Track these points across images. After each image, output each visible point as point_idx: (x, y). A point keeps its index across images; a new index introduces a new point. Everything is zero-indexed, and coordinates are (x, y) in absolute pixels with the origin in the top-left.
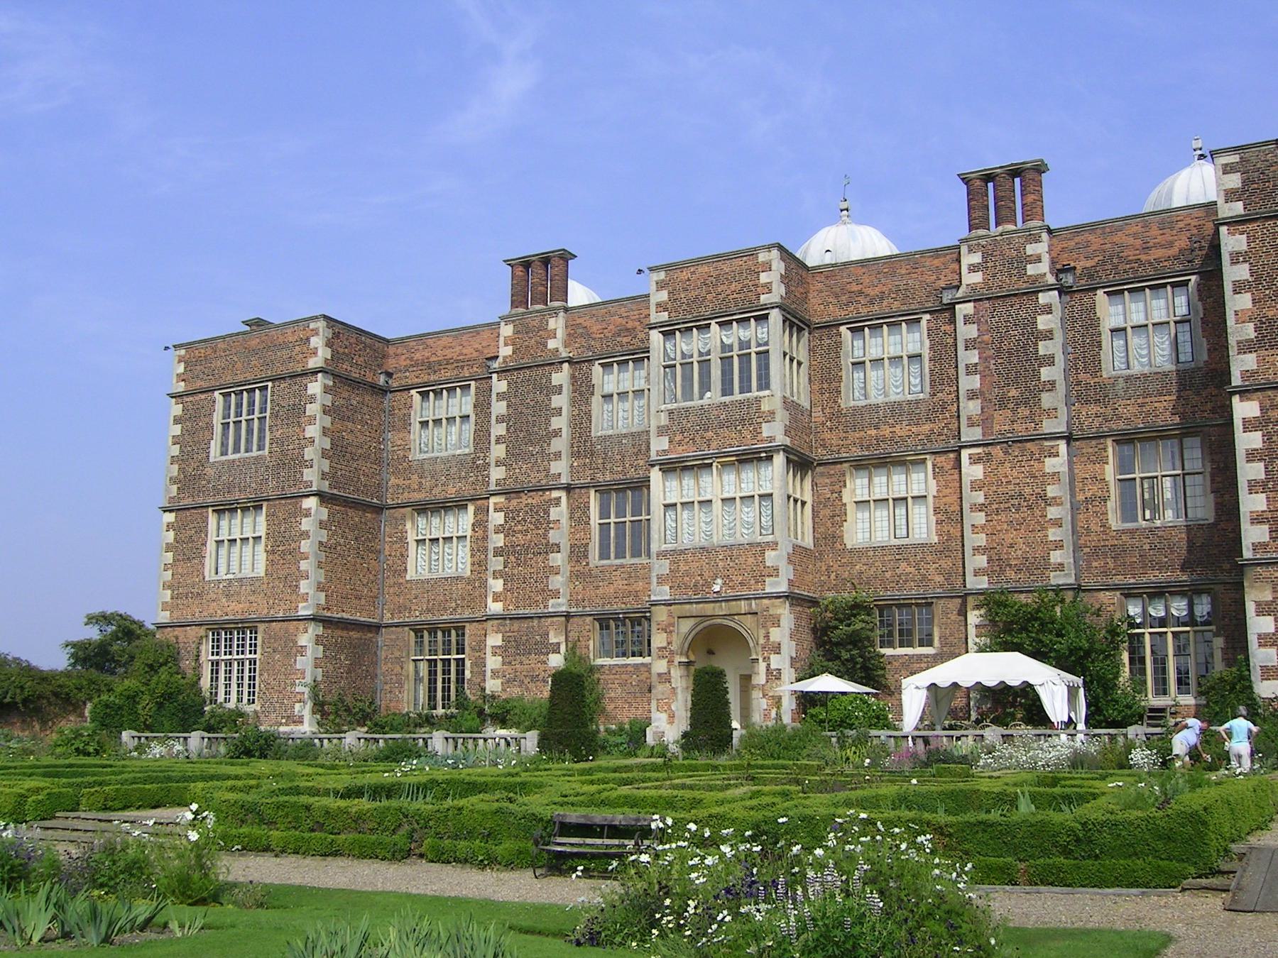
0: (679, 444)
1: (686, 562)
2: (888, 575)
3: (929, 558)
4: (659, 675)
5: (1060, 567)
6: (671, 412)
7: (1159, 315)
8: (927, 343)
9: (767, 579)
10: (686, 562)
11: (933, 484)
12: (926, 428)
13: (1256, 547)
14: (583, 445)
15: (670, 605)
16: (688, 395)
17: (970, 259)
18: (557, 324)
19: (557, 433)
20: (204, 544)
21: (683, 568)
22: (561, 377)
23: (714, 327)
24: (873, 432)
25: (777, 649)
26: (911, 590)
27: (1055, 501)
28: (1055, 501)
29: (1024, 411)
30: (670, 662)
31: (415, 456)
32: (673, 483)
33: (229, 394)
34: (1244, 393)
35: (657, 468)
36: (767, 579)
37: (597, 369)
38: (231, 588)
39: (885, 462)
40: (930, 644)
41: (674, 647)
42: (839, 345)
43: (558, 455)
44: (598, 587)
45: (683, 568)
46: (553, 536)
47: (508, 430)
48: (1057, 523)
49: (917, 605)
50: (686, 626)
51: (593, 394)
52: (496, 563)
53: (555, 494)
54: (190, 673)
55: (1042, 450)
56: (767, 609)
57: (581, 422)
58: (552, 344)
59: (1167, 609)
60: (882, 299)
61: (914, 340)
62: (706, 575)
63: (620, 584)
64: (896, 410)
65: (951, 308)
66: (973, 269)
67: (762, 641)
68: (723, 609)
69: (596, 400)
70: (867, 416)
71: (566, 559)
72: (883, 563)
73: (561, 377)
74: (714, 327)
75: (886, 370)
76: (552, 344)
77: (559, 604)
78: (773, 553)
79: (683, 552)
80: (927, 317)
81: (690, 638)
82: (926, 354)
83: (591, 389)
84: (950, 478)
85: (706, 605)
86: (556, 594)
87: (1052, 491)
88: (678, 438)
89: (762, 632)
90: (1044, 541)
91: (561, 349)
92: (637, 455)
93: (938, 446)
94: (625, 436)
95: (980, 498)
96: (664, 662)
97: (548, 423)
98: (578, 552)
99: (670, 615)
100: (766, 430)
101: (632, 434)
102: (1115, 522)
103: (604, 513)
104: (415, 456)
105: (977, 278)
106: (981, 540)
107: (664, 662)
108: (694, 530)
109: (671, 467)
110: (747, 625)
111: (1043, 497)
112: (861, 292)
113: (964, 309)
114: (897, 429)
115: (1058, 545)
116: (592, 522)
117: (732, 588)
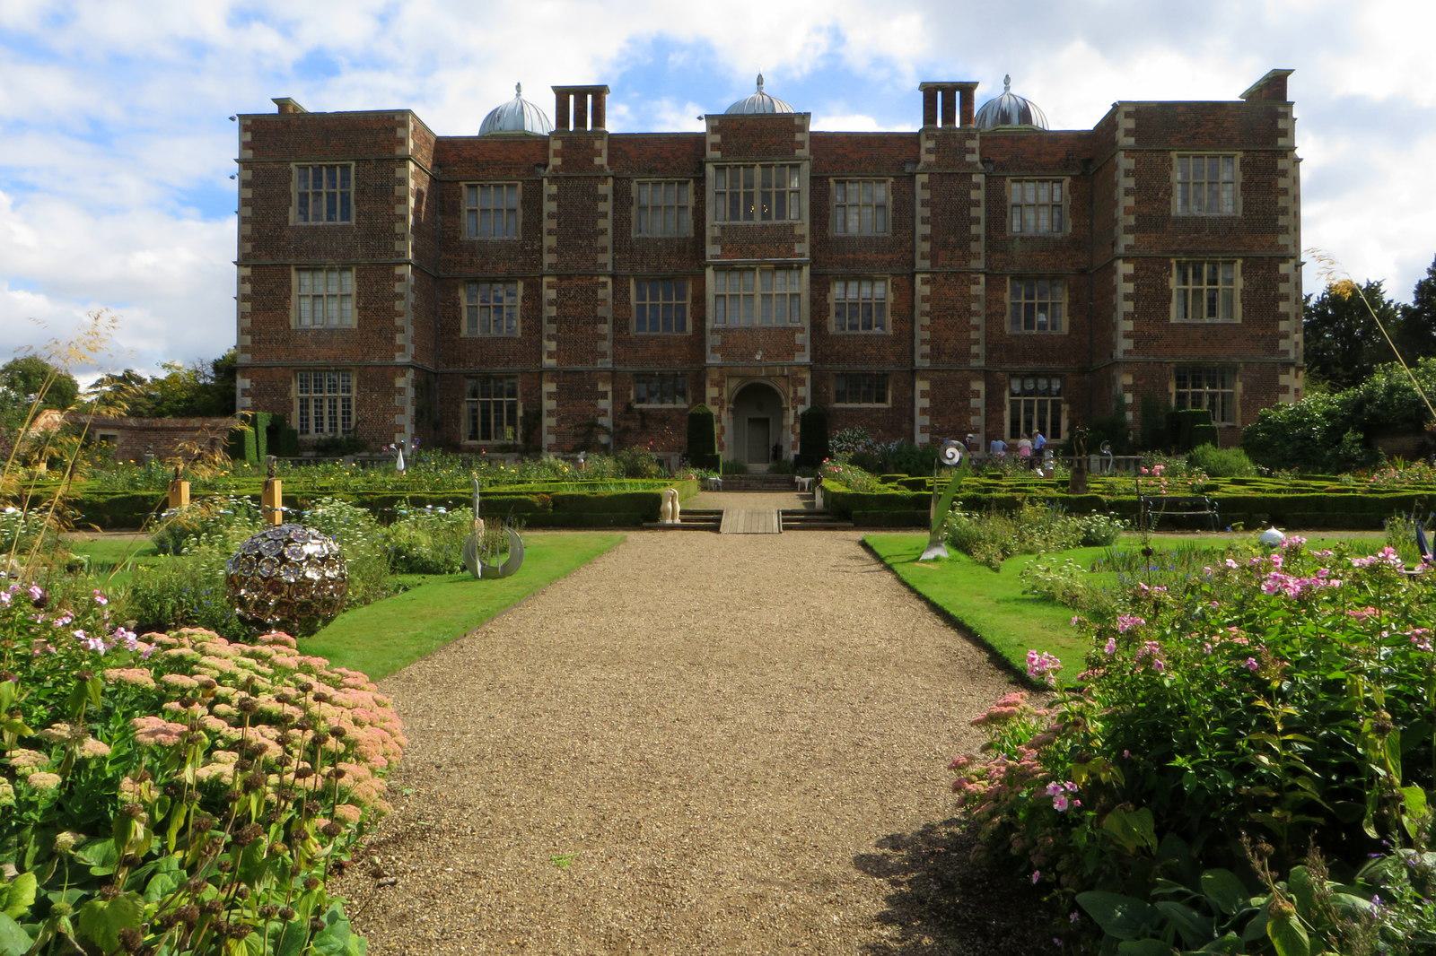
5: (977, 356)
6: (723, 228)
7: (1044, 198)
8: (891, 198)
12: (888, 257)
13: (1125, 352)
16: (735, 216)
20: (288, 297)
24: (852, 256)
27: (976, 314)
28: (976, 314)
29: (958, 253)
31: (465, 237)
33: (306, 168)
34: (1126, 259)
38: (324, 336)
39: (859, 278)
40: (882, 399)
41: (725, 396)
42: (828, 190)
43: (604, 250)
46: (601, 311)
47: (559, 224)
48: (976, 328)
50: (733, 384)
51: (632, 204)
52: (551, 329)
53: (602, 279)
55: (969, 280)
56: (796, 373)
57: (621, 225)
58: (598, 161)
59: (1036, 384)
61: (882, 192)
65: (912, 176)
66: (929, 151)
69: (634, 209)
76: (598, 161)
77: (606, 363)
79: (731, 330)
82: (890, 205)
87: (974, 307)
88: (728, 247)
90: (968, 339)
91: (606, 167)
94: (660, 240)
95: (927, 307)
97: (595, 223)
98: (620, 325)
101: (666, 240)
102: (1008, 329)
103: (641, 297)
104: (465, 237)
105: (932, 158)
106: (927, 335)
108: (739, 318)
109: (719, 268)
110: (779, 385)
111: (969, 310)
115: (977, 342)
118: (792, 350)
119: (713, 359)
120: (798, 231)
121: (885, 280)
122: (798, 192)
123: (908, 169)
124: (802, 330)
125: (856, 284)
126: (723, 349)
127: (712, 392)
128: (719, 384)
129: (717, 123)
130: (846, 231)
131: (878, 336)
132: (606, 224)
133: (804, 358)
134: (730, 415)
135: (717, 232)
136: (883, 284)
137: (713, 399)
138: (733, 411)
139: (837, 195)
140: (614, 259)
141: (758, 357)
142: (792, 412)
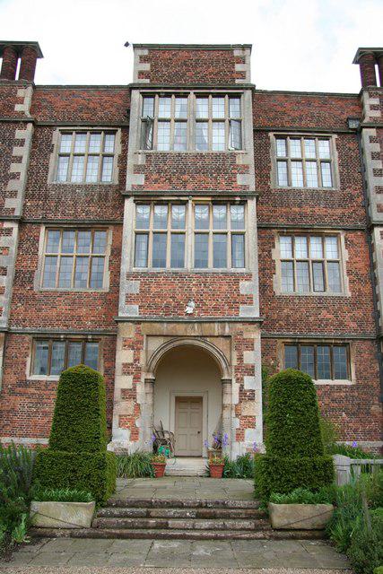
0: (156, 181)
1: (158, 284)
2: (311, 319)
3: (345, 308)
4: (123, 391)
8: (336, 153)
9: (241, 306)
10: (158, 284)
11: (346, 255)
12: (339, 211)
14: (37, 186)
15: (139, 322)
17: (369, 101)
18: (26, 94)
19: (15, 176)
21: (154, 289)
22: (25, 133)
23: (192, 96)
24: (297, 209)
25: (250, 371)
26: (331, 333)
30: (137, 379)
32: (144, 211)
35: (132, 199)
36: (241, 306)
37: (56, 133)
39: (307, 233)
40: (346, 376)
41: (142, 363)
43: (14, 194)
44: (40, 310)
45: (154, 289)
49: (336, 345)
50: (155, 345)
51: (52, 151)
53: (7, 225)
54: (45, 493)
56: (241, 333)
58: (18, 108)
60: (301, 120)
62: (179, 296)
63: (63, 308)
64: (315, 195)
66: (373, 107)
67: (235, 363)
68: (196, 330)
69: (53, 156)
70: (291, 197)
71: (11, 281)
72: (307, 309)
73: (25, 133)
74: (192, 96)
75: (308, 166)
78: (247, 283)
80: (335, 136)
81: (158, 356)
83: (50, 148)
84: (359, 249)
85: (178, 326)
86: (248, 300)
88: (155, 176)
89: (235, 354)
92: (89, 202)
93: (349, 225)
96: (130, 378)
99: (138, 333)
100: (241, 180)
107: (130, 378)
109: (143, 199)
110: (219, 348)
112: (284, 113)
113: (368, 133)
114: (316, 209)
116: (40, 253)
117: (206, 312)
118: (237, 300)
119: (128, 310)
120: (239, 161)
121: (336, 235)
122: (240, 121)
123: (353, 125)
124: (248, 277)
125: (303, 240)
126: (142, 298)
127: (124, 356)
128: (135, 346)
129: (146, 52)
130: (289, 184)
131: (333, 298)
132: (20, 168)
133: (253, 312)
134: (149, 389)
135: (141, 160)
136: (334, 241)
137: (125, 365)
138: (152, 383)
139: (279, 148)
140: (25, 205)
141: (189, 310)
142: (236, 387)
